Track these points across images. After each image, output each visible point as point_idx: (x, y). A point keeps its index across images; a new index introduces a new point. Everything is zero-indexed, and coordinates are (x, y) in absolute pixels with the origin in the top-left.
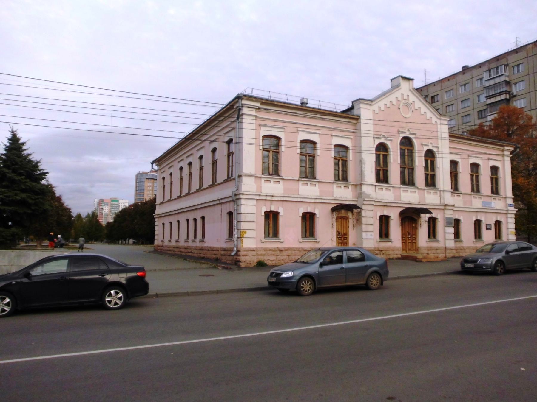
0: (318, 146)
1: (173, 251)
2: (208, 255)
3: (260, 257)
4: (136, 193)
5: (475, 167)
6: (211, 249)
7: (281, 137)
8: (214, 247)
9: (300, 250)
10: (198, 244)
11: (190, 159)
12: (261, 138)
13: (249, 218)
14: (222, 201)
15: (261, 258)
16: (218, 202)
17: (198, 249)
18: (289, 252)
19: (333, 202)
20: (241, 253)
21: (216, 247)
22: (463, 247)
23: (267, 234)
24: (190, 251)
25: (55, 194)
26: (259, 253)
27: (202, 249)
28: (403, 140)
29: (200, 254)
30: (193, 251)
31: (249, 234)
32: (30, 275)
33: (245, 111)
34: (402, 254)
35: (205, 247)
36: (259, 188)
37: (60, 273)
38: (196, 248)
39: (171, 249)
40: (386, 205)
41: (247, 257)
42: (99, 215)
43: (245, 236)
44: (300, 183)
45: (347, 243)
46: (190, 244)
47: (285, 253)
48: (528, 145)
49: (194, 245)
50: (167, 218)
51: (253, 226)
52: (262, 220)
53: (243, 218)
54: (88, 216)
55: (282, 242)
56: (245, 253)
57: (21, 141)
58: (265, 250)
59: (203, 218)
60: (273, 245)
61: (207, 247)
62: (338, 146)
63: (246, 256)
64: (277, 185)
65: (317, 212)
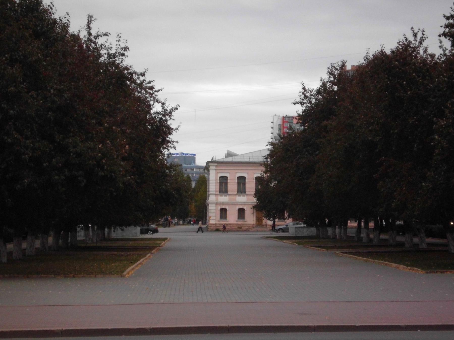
0: (229, 178)
3: (217, 227)
4: (291, 118)
7: (245, 176)
9: (236, 225)
12: (237, 178)
13: (213, 211)
15: (218, 228)
18: (231, 225)
19: (253, 203)
20: (209, 225)
22: (288, 223)
23: (221, 217)
25: (165, 142)
26: (217, 225)
28: (140, 226)
31: (212, 218)
33: (211, 167)
36: (217, 199)
40: (223, 204)
41: (211, 227)
42: (313, 98)
43: (211, 219)
44: (237, 196)
45: (141, 229)
47: (229, 226)
51: (214, 214)
52: (219, 212)
53: (210, 211)
55: (246, 221)
56: (210, 225)
57: (128, 227)
58: (220, 224)
60: (224, 222)
62: (239, 178)
63: (211, 227)
64: (226, 198)
65: (245, 208)
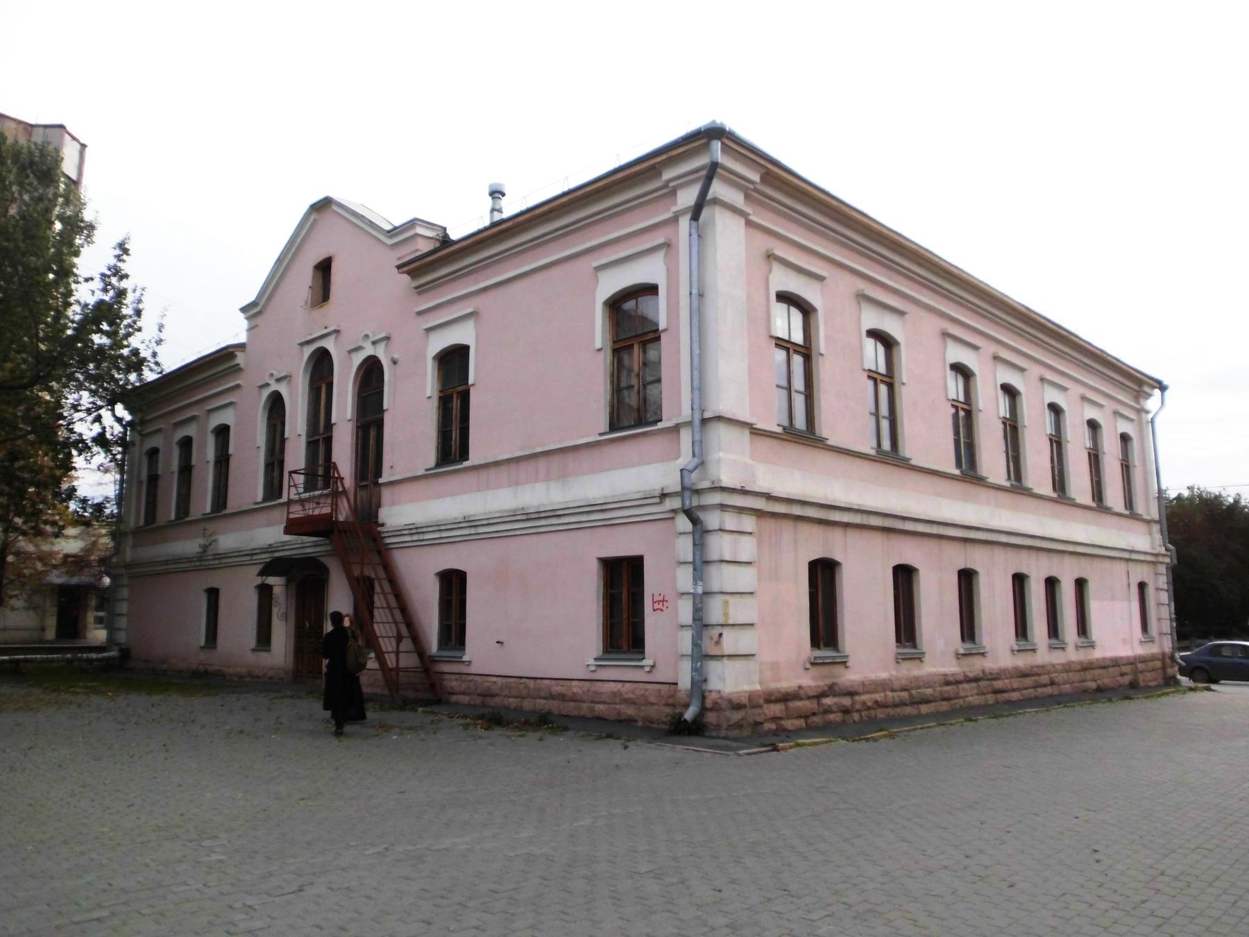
1: (944, 699)
2: (1107, 681)
5: (1051, 584)
6: (1115, 662)
8: (1122, 658)
10: (1072, 655)
11: (191, 430)
14: (1134, 556)
16: (1126, 555)
17: (1079, 667)
21: (1128, 658)
24: (1045, 679)
27: (1087, 667)
29: (1084, 681)
30: (1060, 677)
32: (359, 424)
34: (966, 674)
35: (1098, 660)
37: (480, 232)
38: (1068, 668)
39: (929, 691)
46: (1044, 655)
48: (340, 599)
49: (1058, 658)
50: (1068, 562)
54: (74, 265)
59: (1080, 584)
61: (1104, 658)
